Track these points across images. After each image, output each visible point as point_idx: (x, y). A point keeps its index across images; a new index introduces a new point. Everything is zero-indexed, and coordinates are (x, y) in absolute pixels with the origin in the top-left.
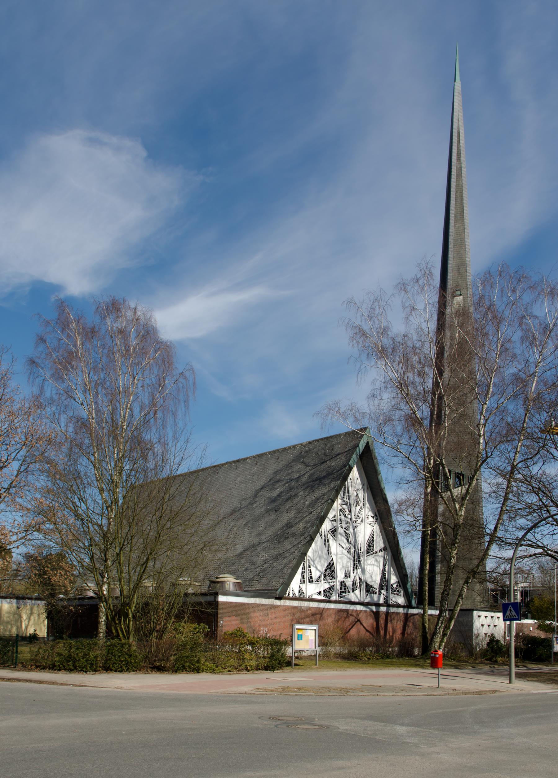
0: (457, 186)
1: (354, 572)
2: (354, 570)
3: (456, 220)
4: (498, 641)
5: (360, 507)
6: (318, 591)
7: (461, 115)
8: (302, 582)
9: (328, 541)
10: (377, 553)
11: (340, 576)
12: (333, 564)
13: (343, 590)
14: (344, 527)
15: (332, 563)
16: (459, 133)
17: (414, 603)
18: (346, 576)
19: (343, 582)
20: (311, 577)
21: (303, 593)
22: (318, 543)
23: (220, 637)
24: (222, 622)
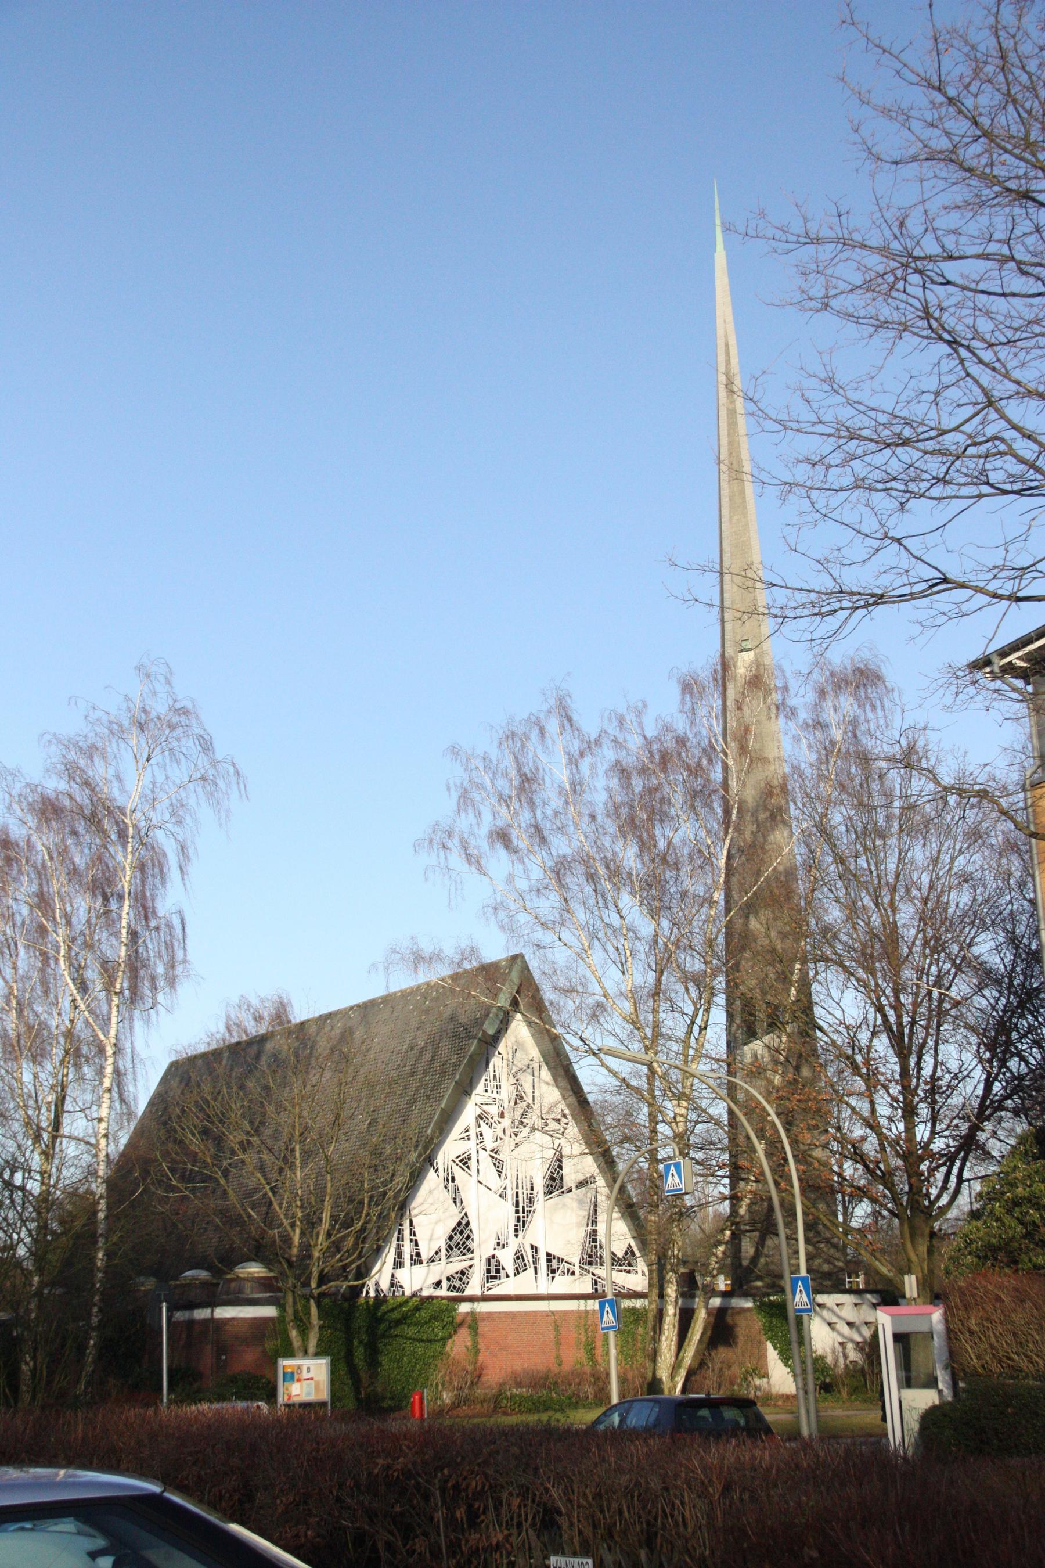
0: (730, 443)
1: (516, 1236)
2: (516, 1230)
3: (733, 509)
4: (822, 1358)
5: (524, 1104)
6: (435, 1280)
7: (729, 311)
8: (398, 1264)
9: (703, 1028)
10: (570, 1191)
11: (483, 1246)
12: (468, 1224)
13: (493, 1273)
14: (489, 1148)
15: (464, 1222)
16: (727, 345)
17: (312, 1349)
18: (498, 1244)
19: (493, 1257)
20: (418, 1255)
21: (401, 1287)
22: (432, 1181)
23: (728, 1468)
24: (224, 1357)
